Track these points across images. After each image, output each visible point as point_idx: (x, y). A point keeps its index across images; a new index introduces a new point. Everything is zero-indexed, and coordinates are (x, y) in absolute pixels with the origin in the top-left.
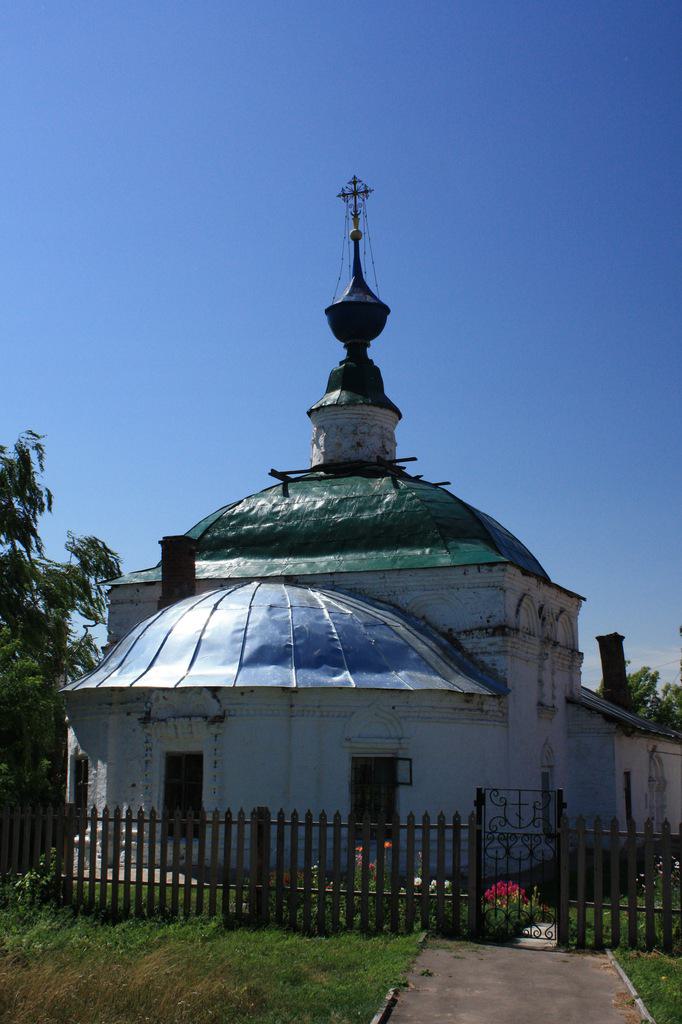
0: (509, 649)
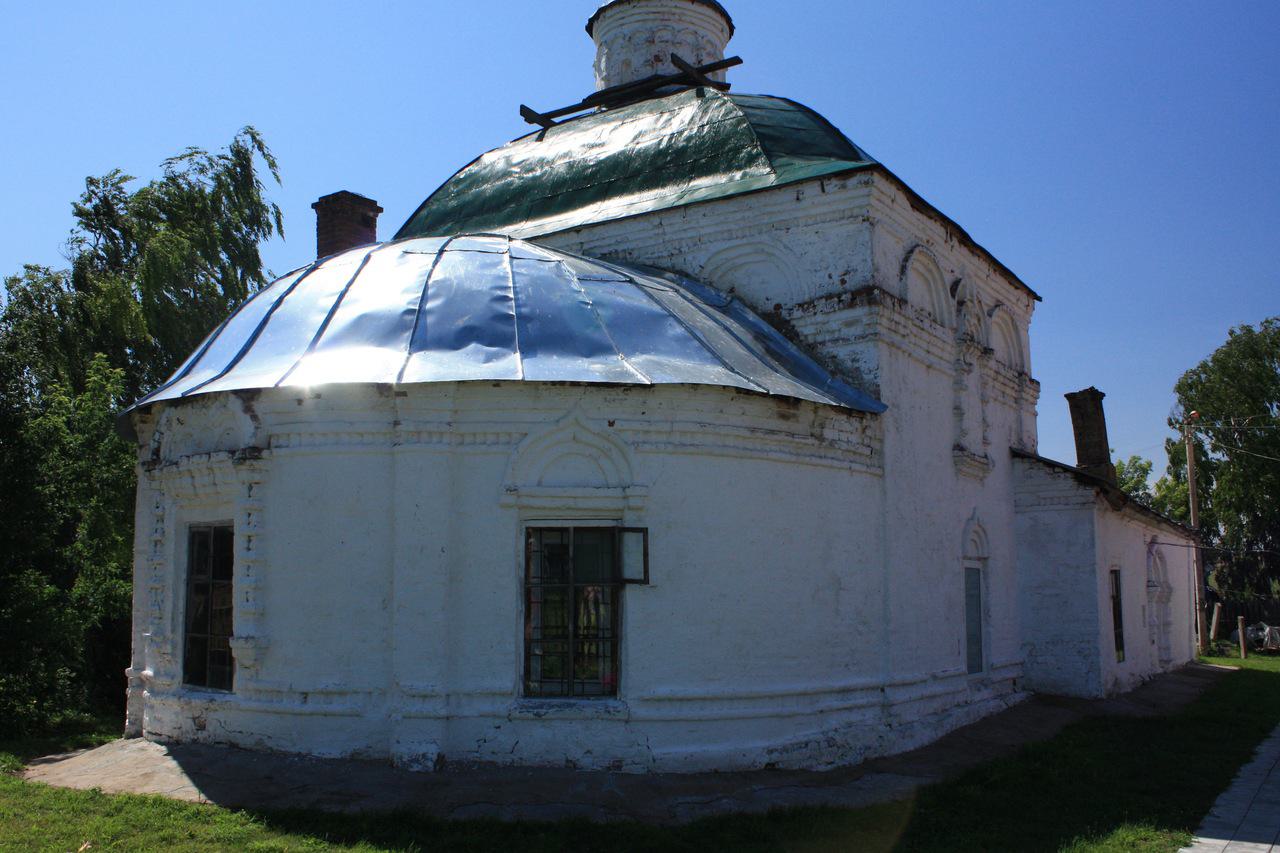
0: (884, 331)
